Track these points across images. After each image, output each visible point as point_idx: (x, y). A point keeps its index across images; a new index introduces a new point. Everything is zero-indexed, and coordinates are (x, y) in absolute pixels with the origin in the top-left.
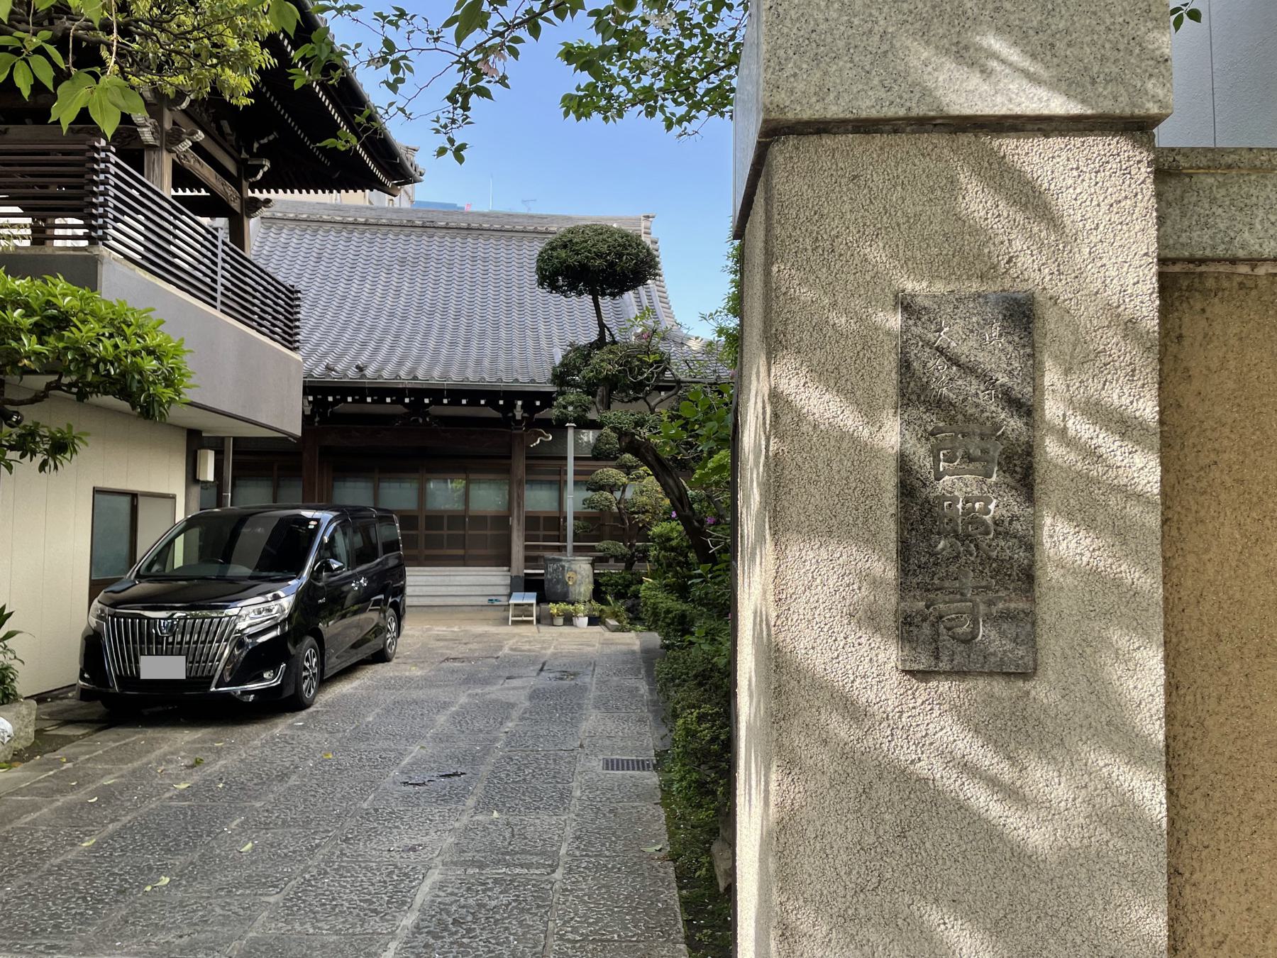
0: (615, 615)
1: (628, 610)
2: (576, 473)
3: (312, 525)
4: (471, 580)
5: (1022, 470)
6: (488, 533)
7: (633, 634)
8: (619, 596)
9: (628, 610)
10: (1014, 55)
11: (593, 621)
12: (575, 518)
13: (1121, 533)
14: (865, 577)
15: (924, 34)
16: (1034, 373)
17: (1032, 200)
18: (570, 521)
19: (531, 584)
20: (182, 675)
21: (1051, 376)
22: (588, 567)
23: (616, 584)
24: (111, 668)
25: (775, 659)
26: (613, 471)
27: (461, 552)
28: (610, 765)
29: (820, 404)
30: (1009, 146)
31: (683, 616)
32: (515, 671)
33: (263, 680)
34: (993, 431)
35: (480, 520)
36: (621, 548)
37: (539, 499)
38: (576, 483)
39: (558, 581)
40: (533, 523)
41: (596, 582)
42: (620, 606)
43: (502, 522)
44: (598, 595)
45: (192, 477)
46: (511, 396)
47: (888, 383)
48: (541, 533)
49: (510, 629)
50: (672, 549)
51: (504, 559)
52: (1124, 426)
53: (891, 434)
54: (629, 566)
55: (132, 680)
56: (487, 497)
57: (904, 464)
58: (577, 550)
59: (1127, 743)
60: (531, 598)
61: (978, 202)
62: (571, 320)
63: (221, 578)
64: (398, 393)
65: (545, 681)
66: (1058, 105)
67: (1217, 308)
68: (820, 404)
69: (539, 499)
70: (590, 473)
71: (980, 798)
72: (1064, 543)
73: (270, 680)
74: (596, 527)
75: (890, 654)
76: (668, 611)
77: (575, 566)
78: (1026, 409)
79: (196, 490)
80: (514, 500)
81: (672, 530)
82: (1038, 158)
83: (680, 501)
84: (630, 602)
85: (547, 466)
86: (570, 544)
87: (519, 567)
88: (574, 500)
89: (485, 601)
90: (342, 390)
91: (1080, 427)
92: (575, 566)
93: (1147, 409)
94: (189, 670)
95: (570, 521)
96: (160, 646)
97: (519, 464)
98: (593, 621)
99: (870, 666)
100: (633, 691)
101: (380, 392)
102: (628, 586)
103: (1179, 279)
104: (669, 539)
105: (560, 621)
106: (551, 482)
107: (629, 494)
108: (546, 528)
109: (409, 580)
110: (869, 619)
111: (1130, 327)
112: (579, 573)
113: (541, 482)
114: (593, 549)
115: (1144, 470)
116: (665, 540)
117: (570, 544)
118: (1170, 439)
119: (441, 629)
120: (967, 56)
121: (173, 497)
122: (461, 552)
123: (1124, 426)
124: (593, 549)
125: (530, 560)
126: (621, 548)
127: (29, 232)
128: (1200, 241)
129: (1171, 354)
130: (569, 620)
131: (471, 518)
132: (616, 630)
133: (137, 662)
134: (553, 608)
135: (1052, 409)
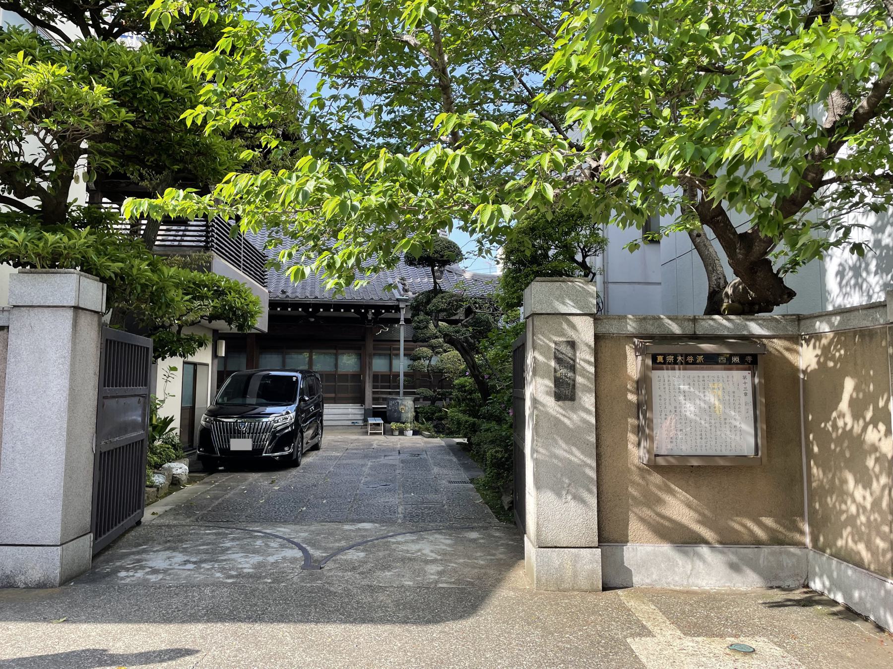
0: (428, 430)
1: (434, 427)
2: (405, 349)
3: (294, 379)
4: (341, 411)
5: (573, 368)
6: (349, 384)
7: (439, 439)
8: (428, 419)
9: (434, 427)
10: (572, 304)
11: (415, 433)
12: (405, 375)
13: (588, 379)
14: (547, 386)
15: (557, 300)
16: (575, 355)
17: (573, 327)
18: (402, 377)
19: (376, 413)
20: (250, 449)
21: (578, 354)
22: (412, 403)
23: (427, 413)
24: (217, 445)
25: (535, 401)
26: (425, 349)
27: (333, 395)
28: (450, 482)
29: (540, 358)
30: (571, 318)
31: (474, 424)
32: (386, 454)
33: (284, 451)
34: (568, 363)
35: (344, 377)
36: (429, 393)
37: (379, 365)
38: (405, 355)
39: (395, 411)
40: (378, 379)
41: (415, 411)
42: (430, 425)
43: (357, 378)
44: (416, 418)
45: (215, 355)
46: (368, 307)
47: (552, 355)
48: (380, 384)
49: (368, 437)
50: (465, 391)
51: (359, 399)
52: (589, 362)
53: (553, 363)
54: (433, 403)
55: (226, 451)
56: (348, 362)
57: (555, 369)
58: (405, 394)
59: (587, 411)
60: (379, 421)
61: (565, 326)
62: (420, 280)
63: (245, 405)
64: (305, 306)
65: (403, 456)
66: (579, 312)
67: (607, 341)
68: (540, 358)
69: (379, 365)
70: (413, 349)
71: (562, 418)
72: (579, 380)
73: (287, 451)
74: (415, 379)
75: (553, 399)
76: (467, 421)
77: (405, 403)
78: (574, 361)
79: (216, 361)
80: (364, 364)
81: (466, 381)
82: (574, 319)
83: (473, 367)
84: (435, 423)
85: (388, 348)
86: (402, 390)
87: (369, 403)
88: (401, 365)
89: (350, 423)
90: (284, 305)
91: (582, 363)
92: (405, 403)
93: (592, 360)
94: (253, 446)
95: (402, 377)
96: (239, 434)
97: (370, 344)
98: (415, 433)
99: (550, 403)
100: (450, 461)
101: (295, 305)
102: (433, 414)
103: (597, 337)
104: (464, 386)
105: (397, 433)
106: (385, 355)
107: (433, 363)
108: (388, 381)
109: (325, 411)
110: (548, 393)
111: (589, 346)
112: (407, 406)
113: (380, 355)
114: (414, 393)
115: (592, 369)
116: (462, 387)
117: (402, 390)
118: (596, 365)
119: (339, 437)
120: (564, 303)
121: (208, 365)
122: (333, 395)
123: (589, 362)
124: (414, 393)
125: (375, 400)
126: (429, 393)
127: (129, 227)
128: (602, 330)
129: (596, 352)
130: (402, 432)
131: (340, 375)
132: (429, 437)
133: (229, 442)
134: (393, 425)
135: (578, 360)
